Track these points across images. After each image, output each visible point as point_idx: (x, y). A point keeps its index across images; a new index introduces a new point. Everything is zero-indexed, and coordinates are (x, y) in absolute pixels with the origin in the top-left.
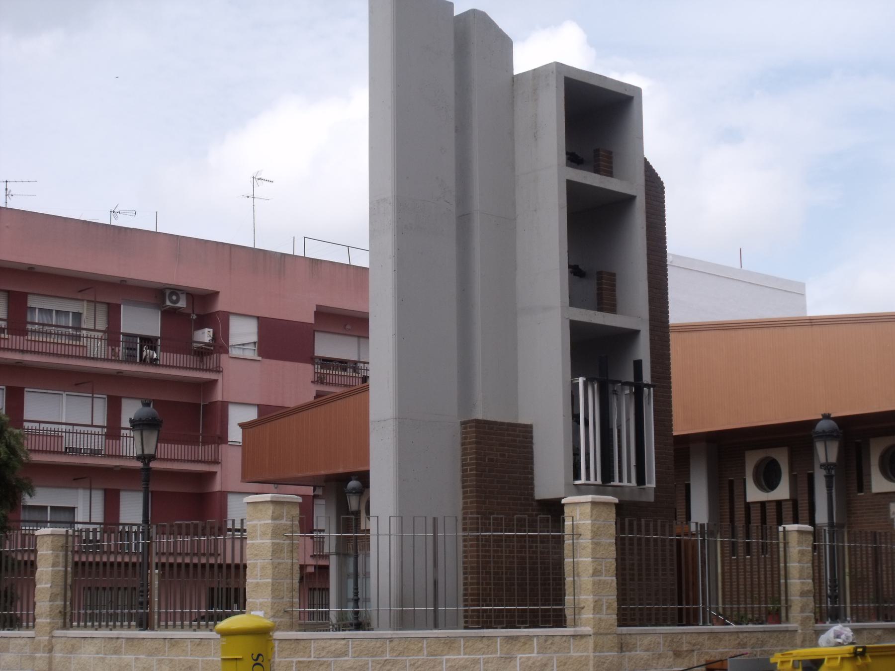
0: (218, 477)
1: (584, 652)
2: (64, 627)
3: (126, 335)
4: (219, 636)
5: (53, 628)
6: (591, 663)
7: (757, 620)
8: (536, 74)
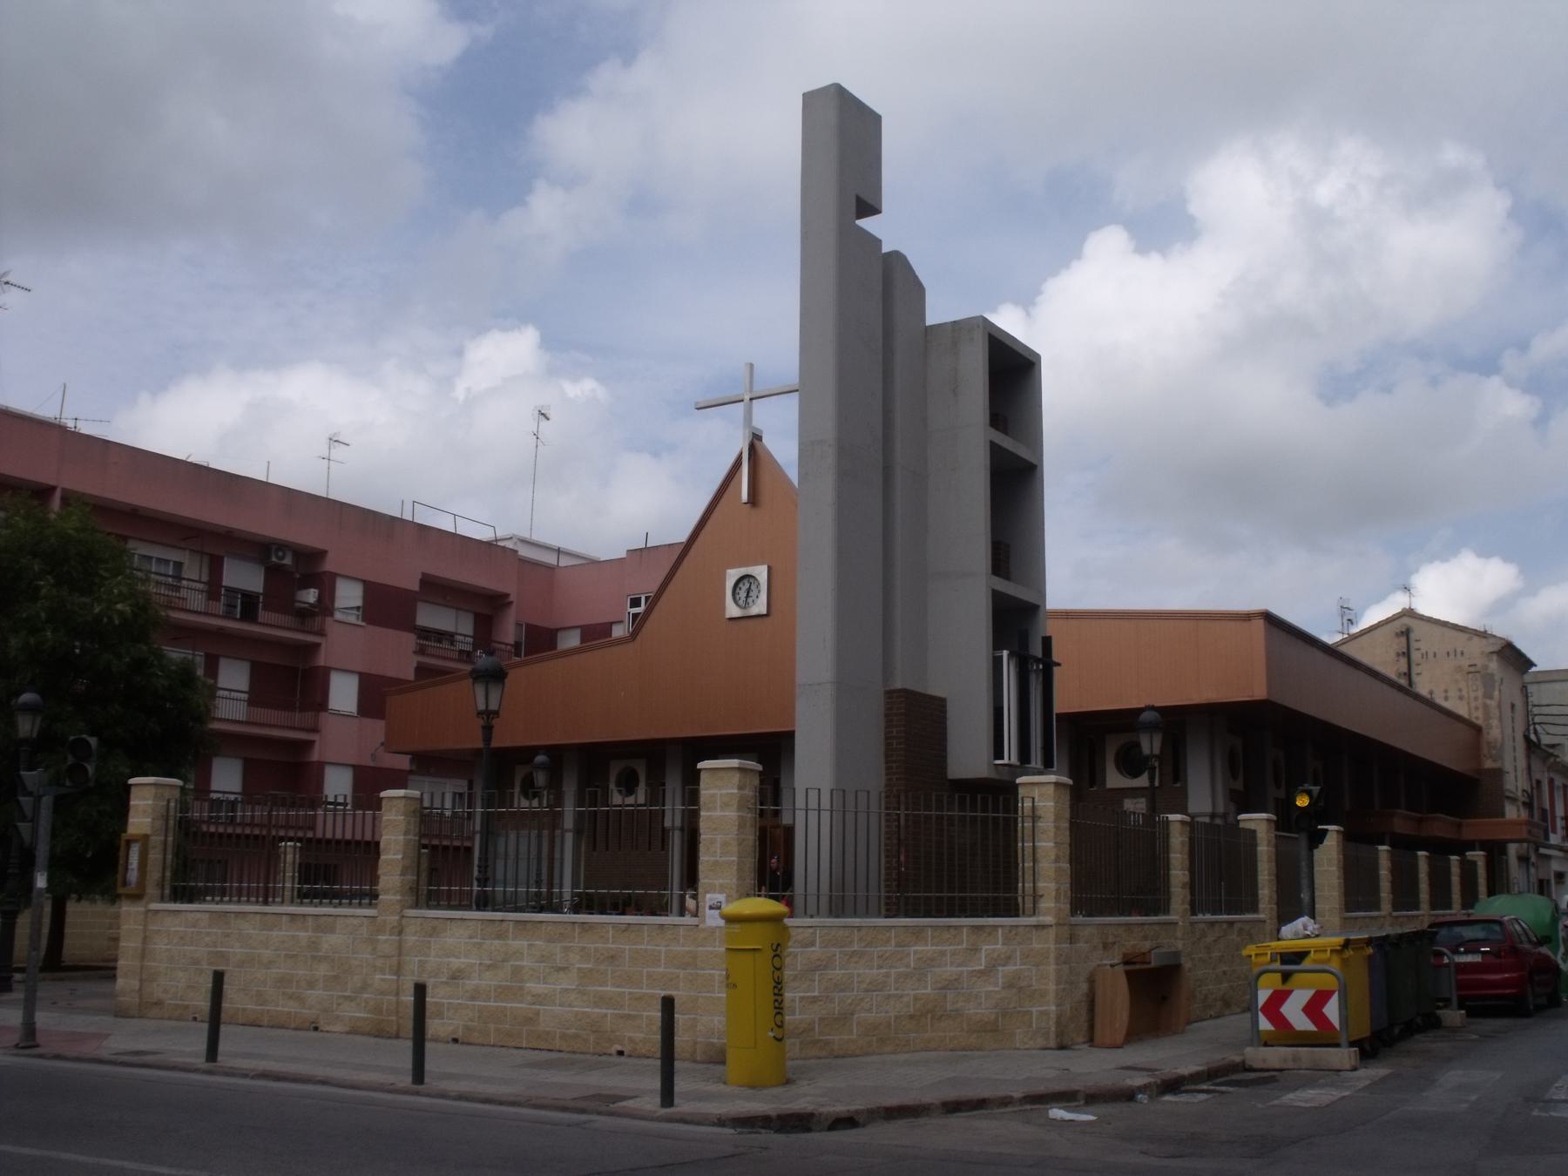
0: (317, 746)
1: (1046, 944)
2: (417, 905)
3: (228, 589)
4: (722, 923)
5: (403, 907)
6: (1052, 956)
7: (505, 902)
8: (957, 329)
